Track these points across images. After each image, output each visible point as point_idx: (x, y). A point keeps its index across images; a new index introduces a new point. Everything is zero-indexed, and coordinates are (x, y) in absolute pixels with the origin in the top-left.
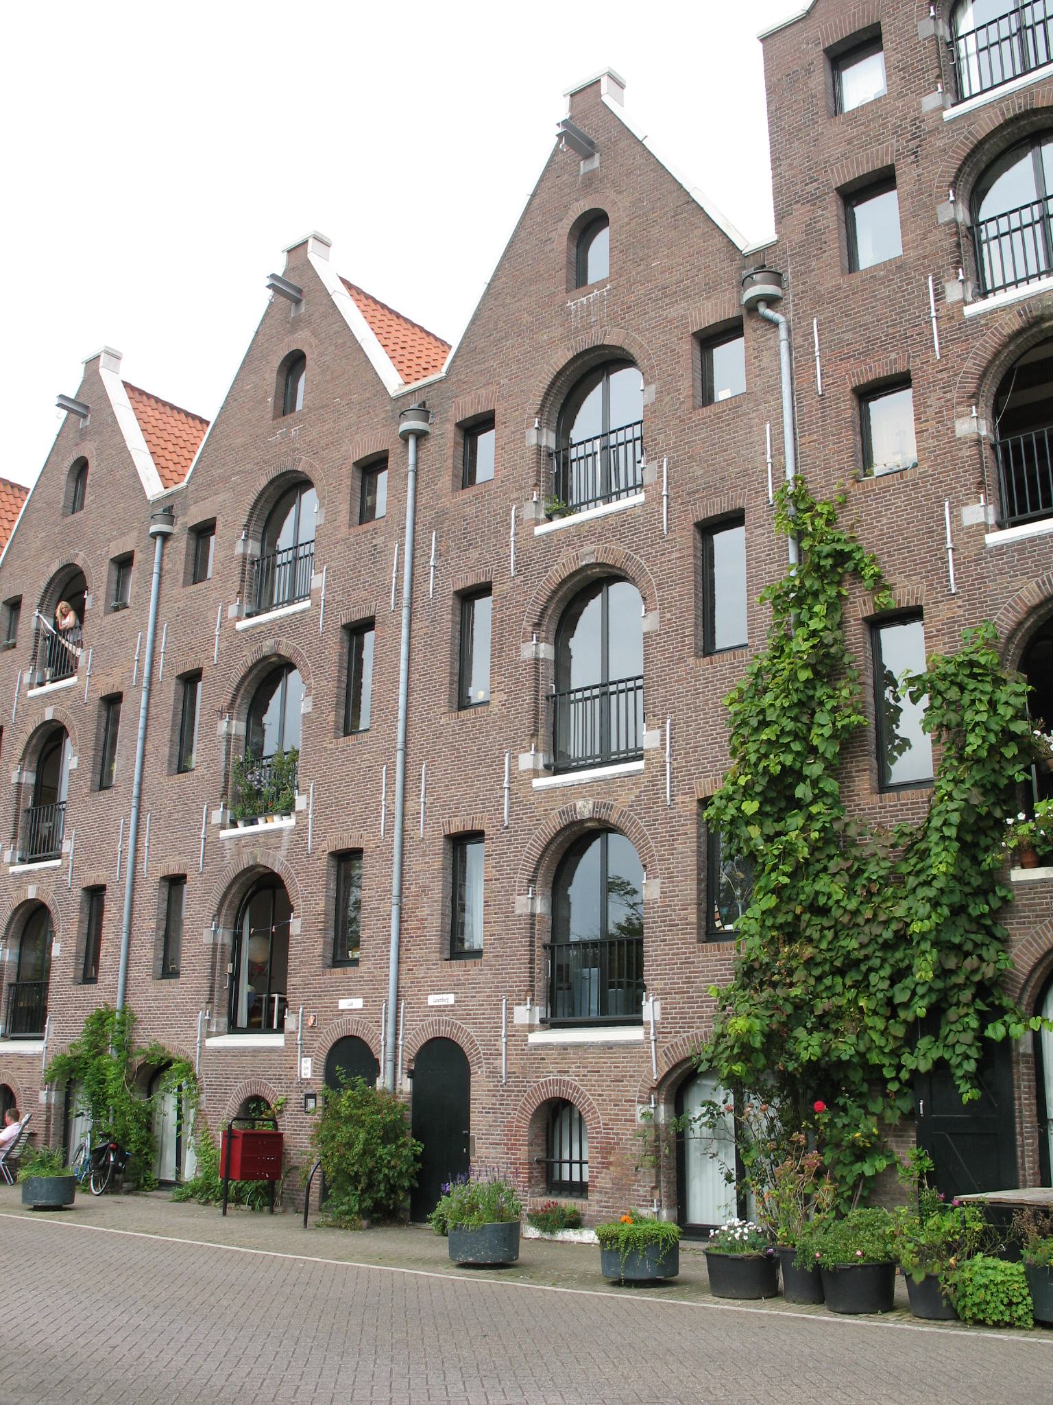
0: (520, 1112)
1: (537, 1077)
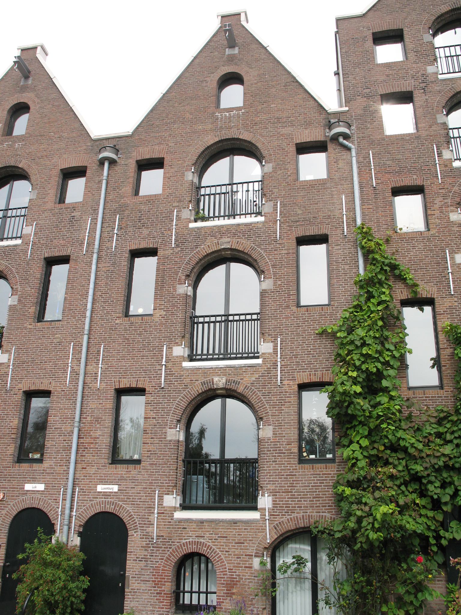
0: (166, 561)
1: (179, 539)
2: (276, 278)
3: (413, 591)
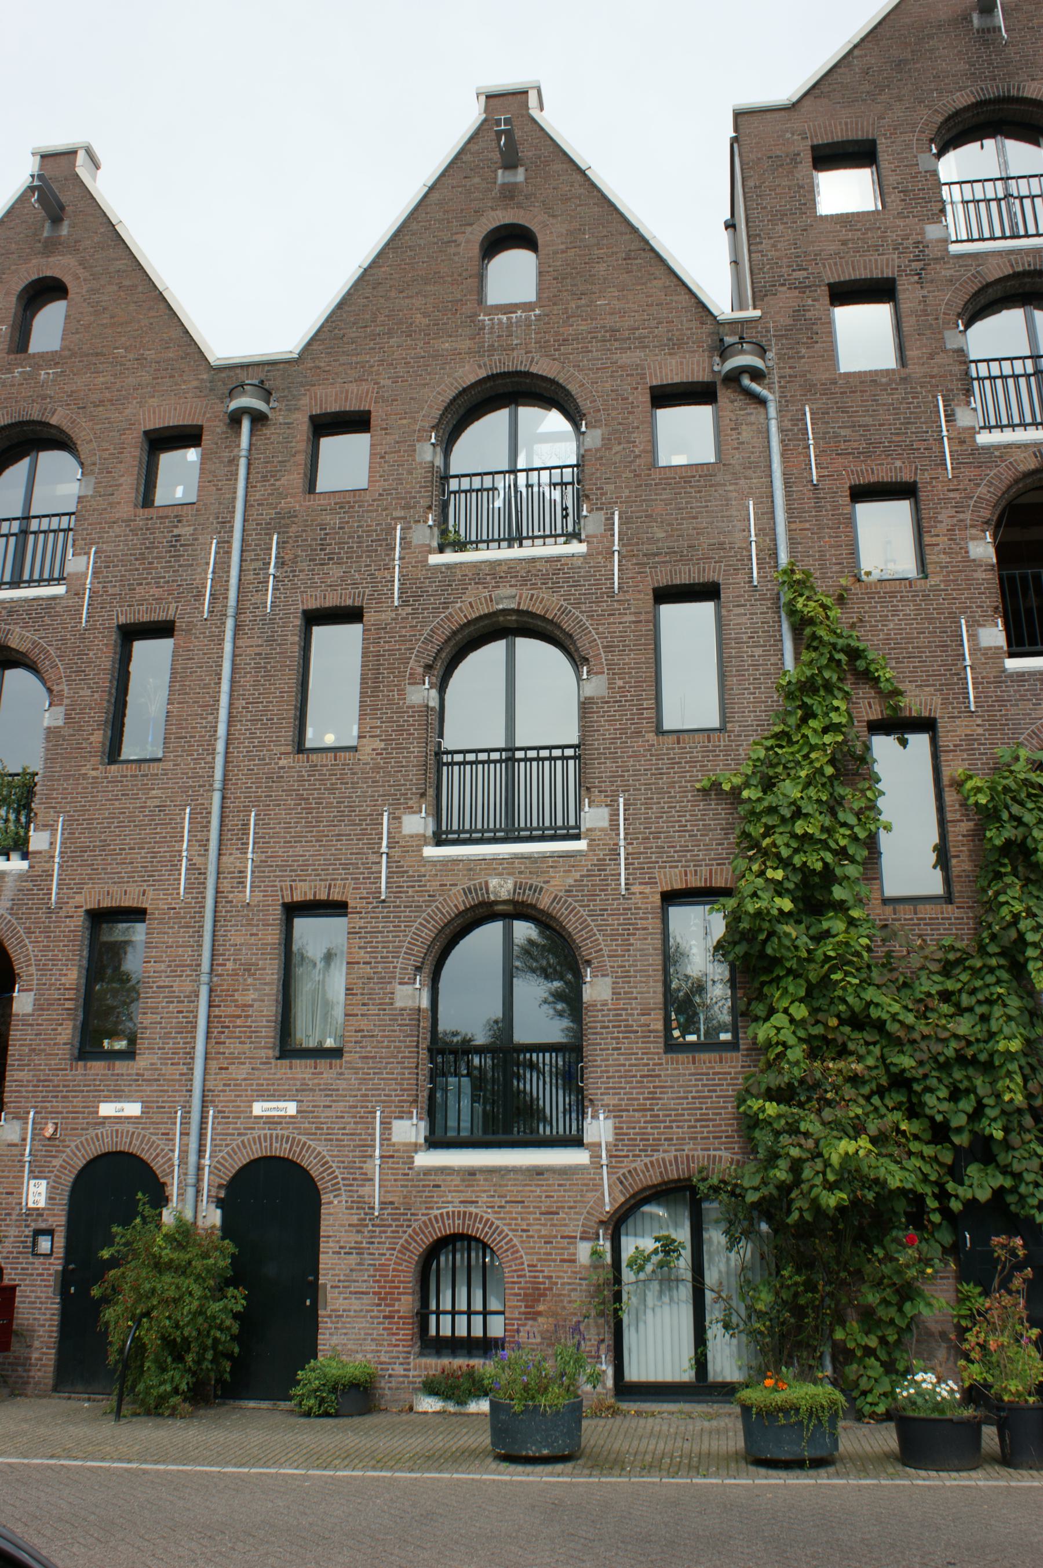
0: (400, 1252)
1: (427, 1208)
3: (894, 1299)
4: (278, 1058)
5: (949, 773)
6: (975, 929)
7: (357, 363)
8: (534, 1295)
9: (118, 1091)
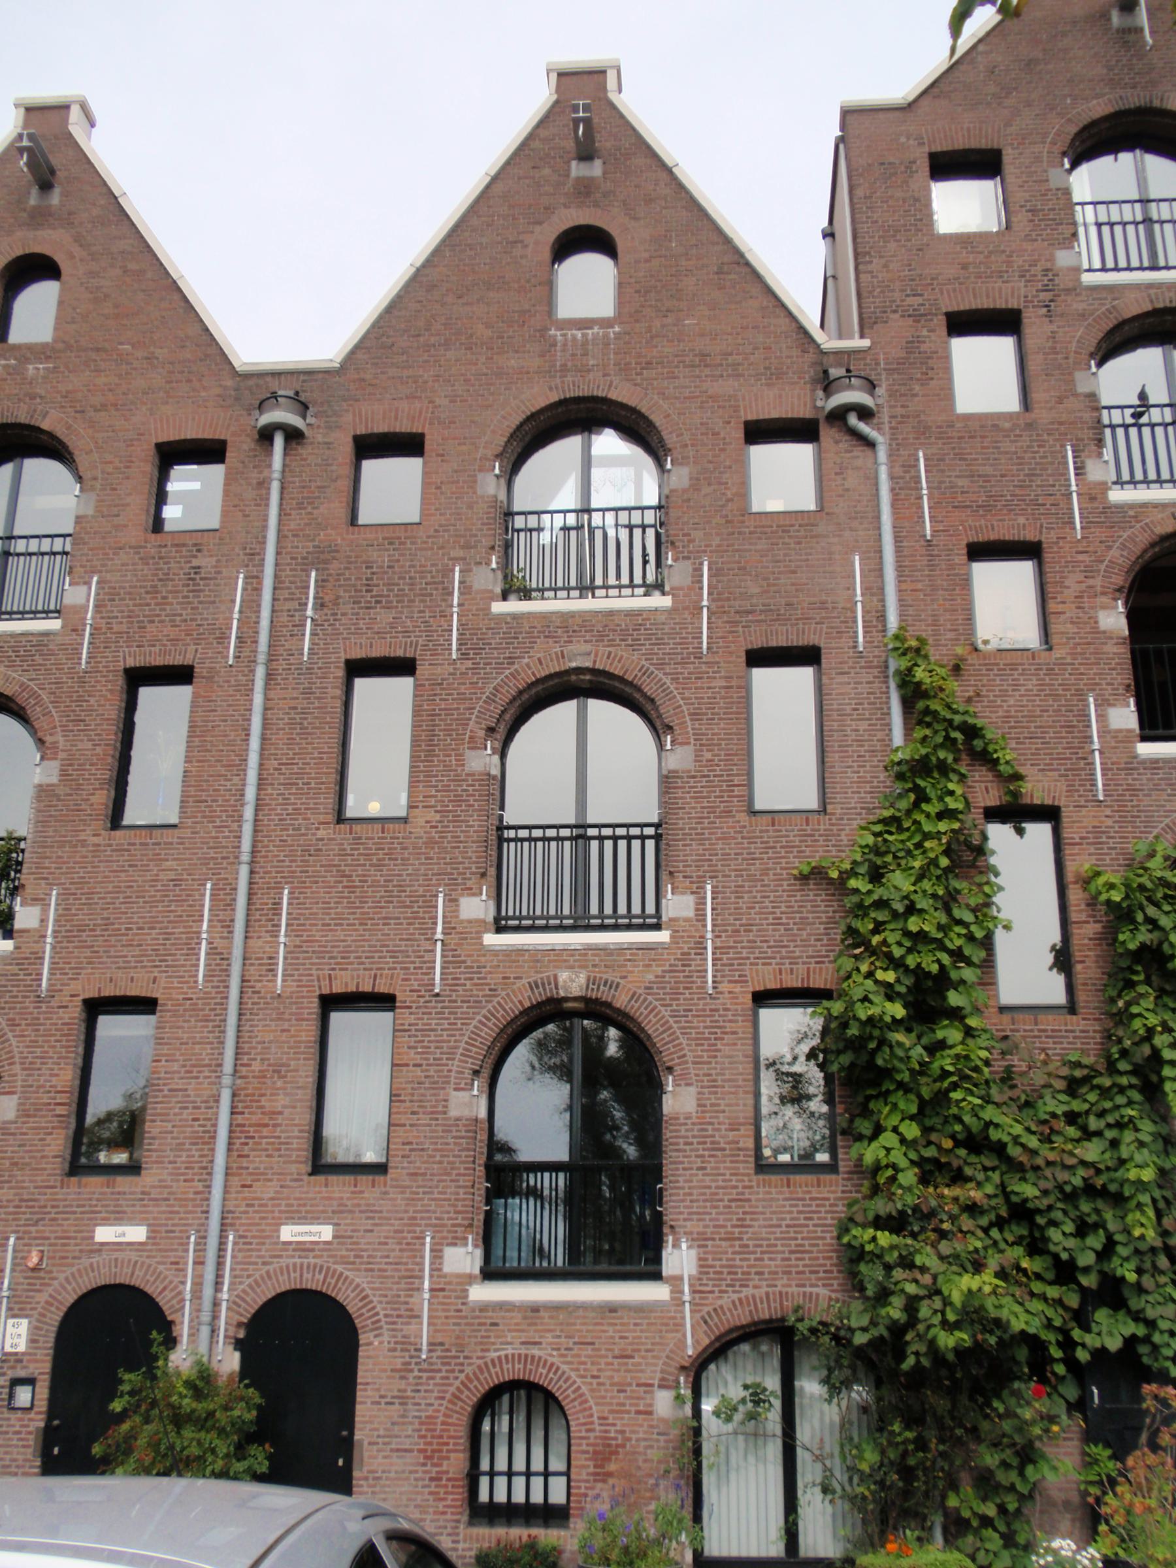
0: (450, 1401)
1: (483, 1350)
2: (701, 745)
3: (1015, 1462)
4: (310, 1175)
5: (1074, 869)
6: (1102, 1044)
7: (408, 377)
8: (604, 1454)
9: (118, 1212)
